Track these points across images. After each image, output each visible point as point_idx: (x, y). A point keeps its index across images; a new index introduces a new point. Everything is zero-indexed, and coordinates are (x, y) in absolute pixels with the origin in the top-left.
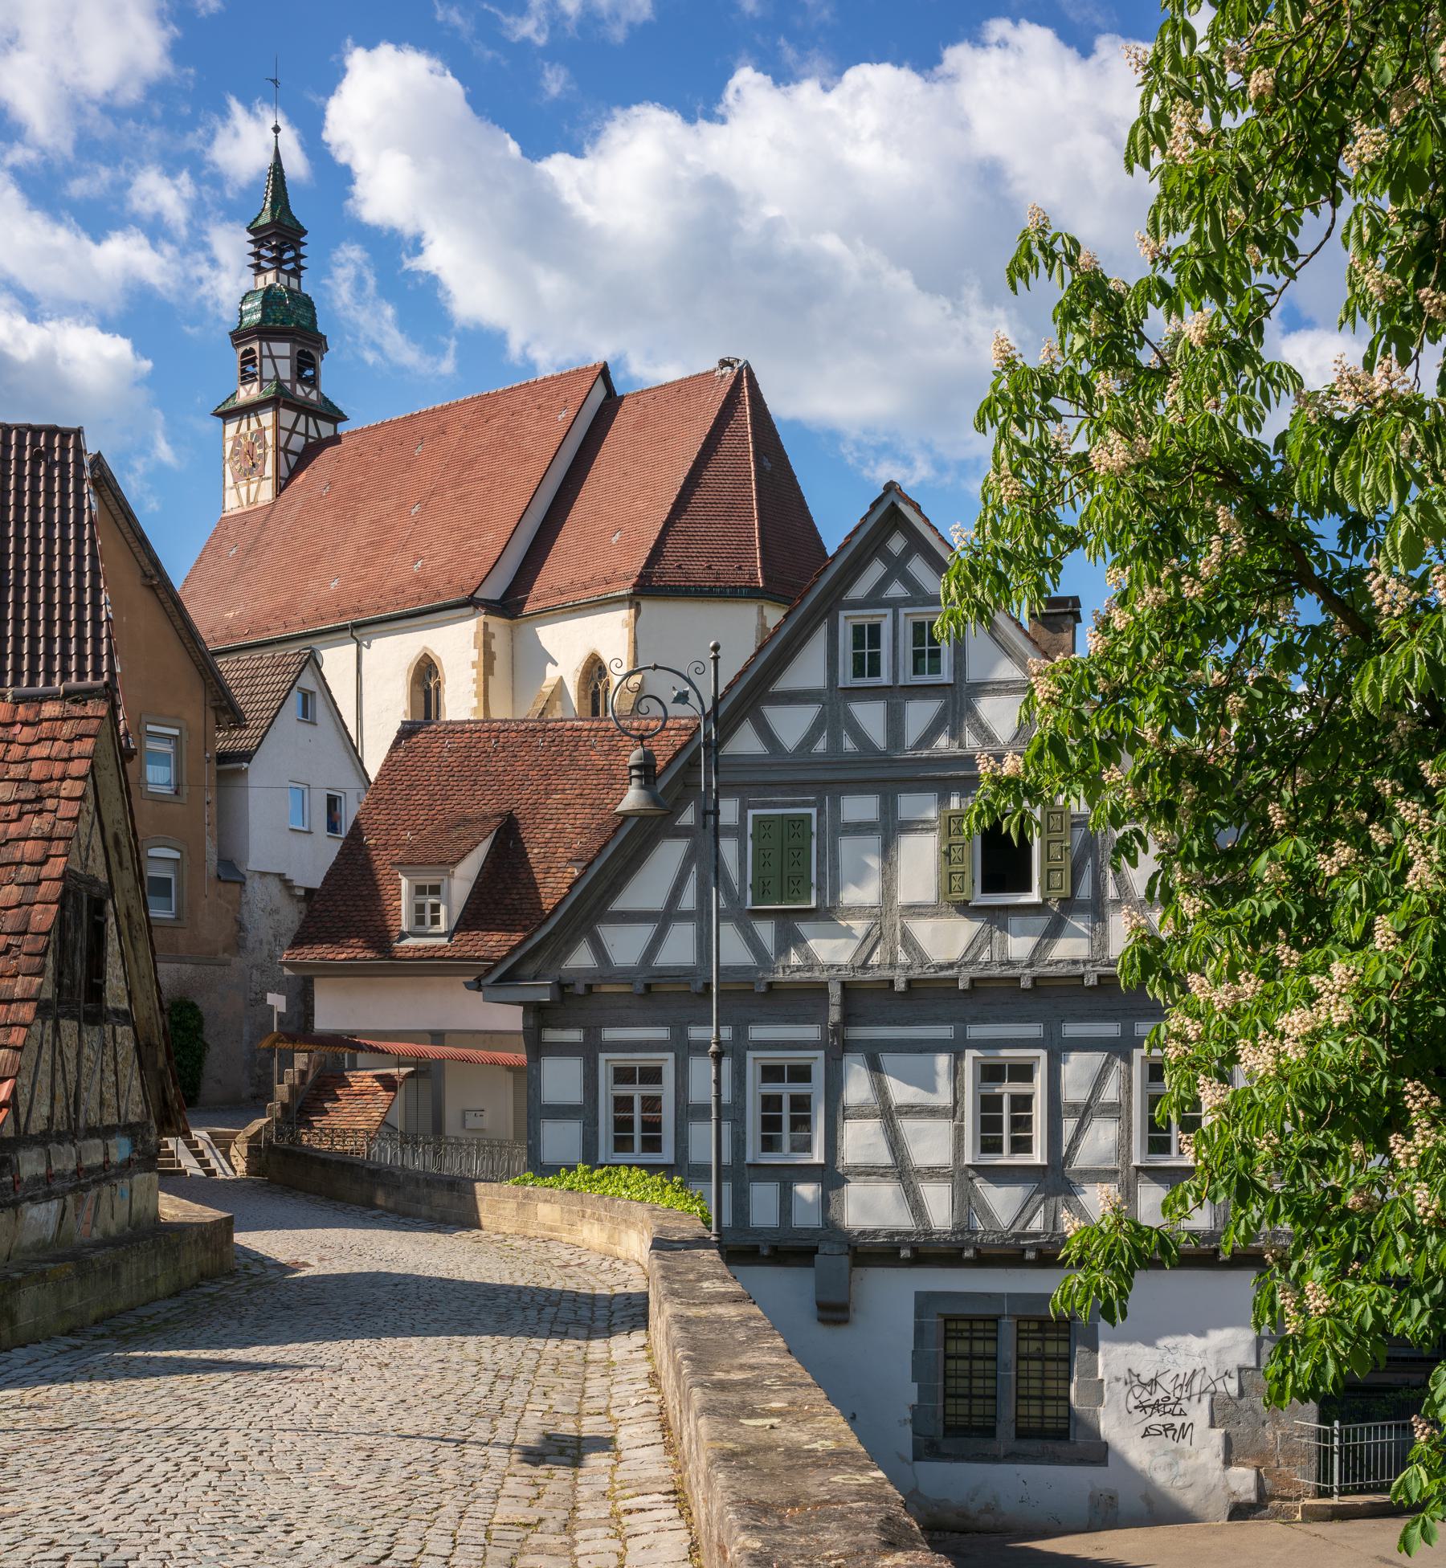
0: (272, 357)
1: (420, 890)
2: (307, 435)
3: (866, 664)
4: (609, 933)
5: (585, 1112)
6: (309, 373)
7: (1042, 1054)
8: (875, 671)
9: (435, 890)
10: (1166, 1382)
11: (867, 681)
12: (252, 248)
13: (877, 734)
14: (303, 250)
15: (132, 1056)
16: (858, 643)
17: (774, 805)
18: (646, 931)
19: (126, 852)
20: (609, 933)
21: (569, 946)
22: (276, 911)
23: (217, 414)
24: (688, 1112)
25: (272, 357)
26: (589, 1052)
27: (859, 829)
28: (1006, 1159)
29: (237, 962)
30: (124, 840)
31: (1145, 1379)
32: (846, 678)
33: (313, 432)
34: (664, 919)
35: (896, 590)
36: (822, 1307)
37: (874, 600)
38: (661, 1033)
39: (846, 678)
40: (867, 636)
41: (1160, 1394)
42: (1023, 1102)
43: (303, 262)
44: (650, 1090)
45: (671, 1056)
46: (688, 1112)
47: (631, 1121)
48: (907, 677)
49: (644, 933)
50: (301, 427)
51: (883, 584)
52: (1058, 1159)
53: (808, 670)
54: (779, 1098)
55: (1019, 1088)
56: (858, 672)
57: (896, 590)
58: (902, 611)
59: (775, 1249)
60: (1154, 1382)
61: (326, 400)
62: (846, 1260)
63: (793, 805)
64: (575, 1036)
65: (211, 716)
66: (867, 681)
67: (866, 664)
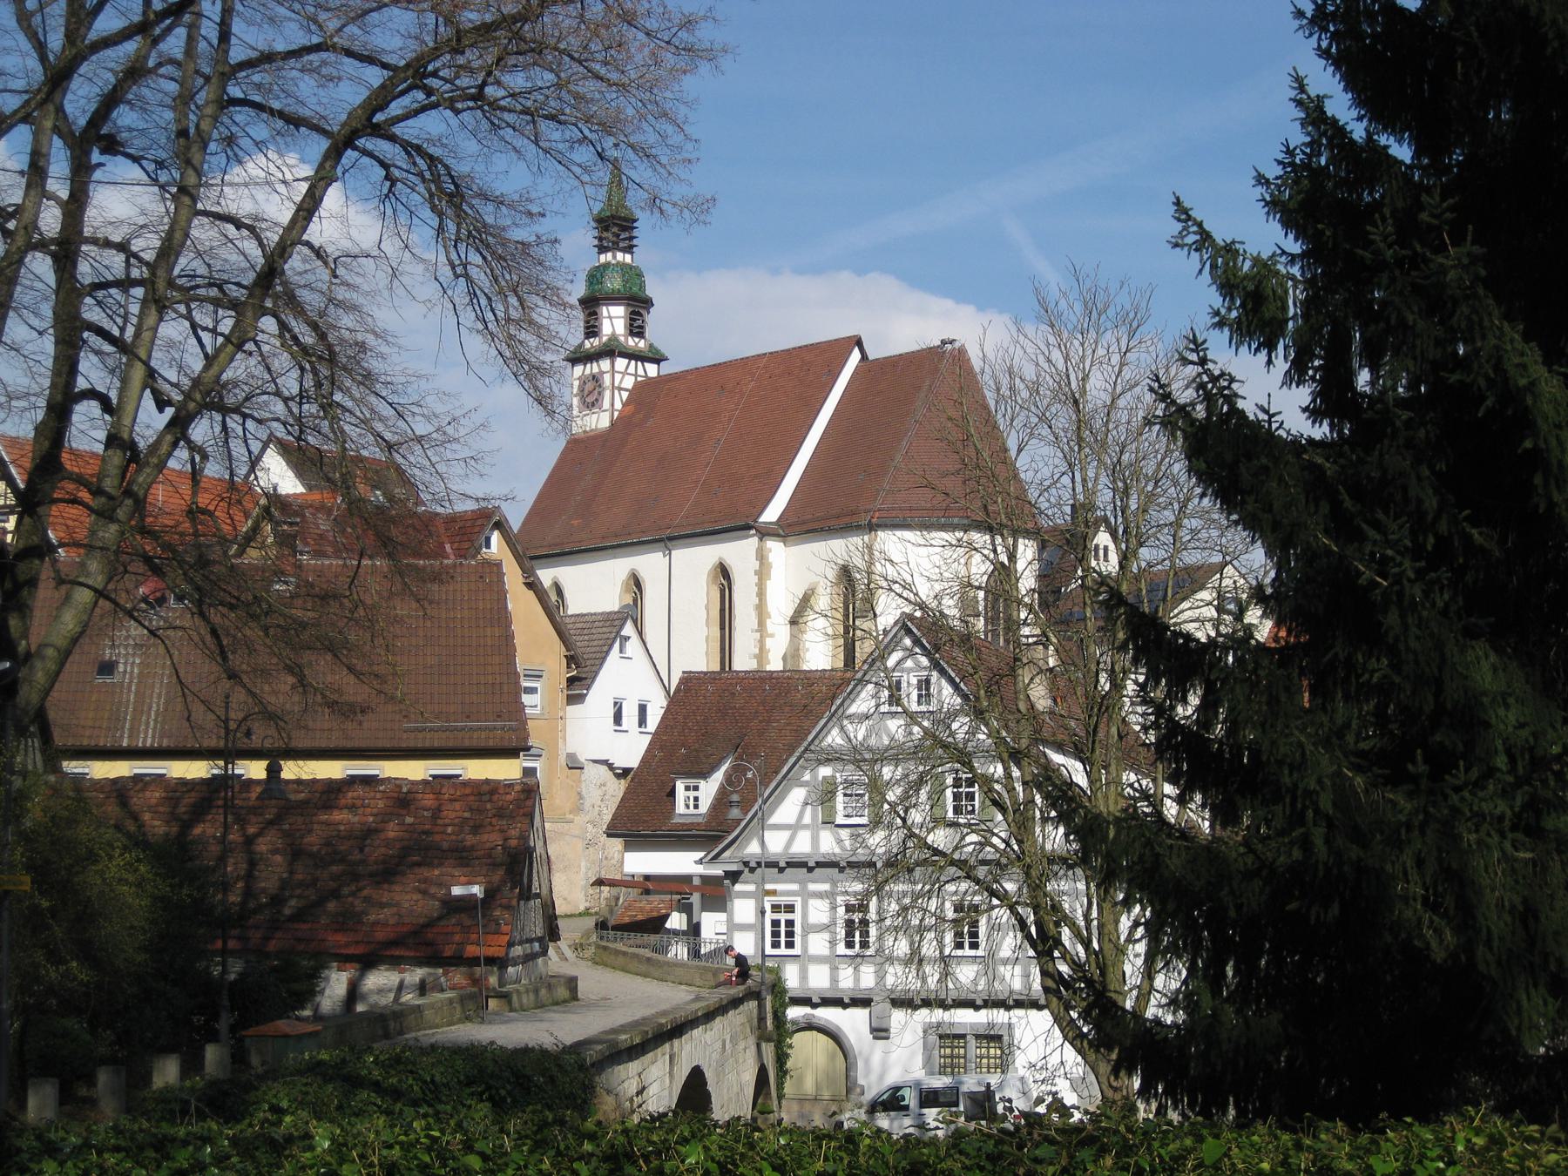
0: (610, 318)
1: (687, 788)
2: (636, 375)
9: (696, 788)
15: (991, 1025)
18: (786, 834)
21: (748, 841)
25: (610, 318)
29: (577, 819)
33: (641, 372)
34: (795, 828)
36: (874, 1030)
38: (795, 887)
42: (790, 923)
43: (635, 242)
44: (790, 916)
46: (808, 929)
49: (784, 835)
50: (631, 370)
52: (992, 954)
55: (790, 916)
61: (651, 346)
64: (751, 888)
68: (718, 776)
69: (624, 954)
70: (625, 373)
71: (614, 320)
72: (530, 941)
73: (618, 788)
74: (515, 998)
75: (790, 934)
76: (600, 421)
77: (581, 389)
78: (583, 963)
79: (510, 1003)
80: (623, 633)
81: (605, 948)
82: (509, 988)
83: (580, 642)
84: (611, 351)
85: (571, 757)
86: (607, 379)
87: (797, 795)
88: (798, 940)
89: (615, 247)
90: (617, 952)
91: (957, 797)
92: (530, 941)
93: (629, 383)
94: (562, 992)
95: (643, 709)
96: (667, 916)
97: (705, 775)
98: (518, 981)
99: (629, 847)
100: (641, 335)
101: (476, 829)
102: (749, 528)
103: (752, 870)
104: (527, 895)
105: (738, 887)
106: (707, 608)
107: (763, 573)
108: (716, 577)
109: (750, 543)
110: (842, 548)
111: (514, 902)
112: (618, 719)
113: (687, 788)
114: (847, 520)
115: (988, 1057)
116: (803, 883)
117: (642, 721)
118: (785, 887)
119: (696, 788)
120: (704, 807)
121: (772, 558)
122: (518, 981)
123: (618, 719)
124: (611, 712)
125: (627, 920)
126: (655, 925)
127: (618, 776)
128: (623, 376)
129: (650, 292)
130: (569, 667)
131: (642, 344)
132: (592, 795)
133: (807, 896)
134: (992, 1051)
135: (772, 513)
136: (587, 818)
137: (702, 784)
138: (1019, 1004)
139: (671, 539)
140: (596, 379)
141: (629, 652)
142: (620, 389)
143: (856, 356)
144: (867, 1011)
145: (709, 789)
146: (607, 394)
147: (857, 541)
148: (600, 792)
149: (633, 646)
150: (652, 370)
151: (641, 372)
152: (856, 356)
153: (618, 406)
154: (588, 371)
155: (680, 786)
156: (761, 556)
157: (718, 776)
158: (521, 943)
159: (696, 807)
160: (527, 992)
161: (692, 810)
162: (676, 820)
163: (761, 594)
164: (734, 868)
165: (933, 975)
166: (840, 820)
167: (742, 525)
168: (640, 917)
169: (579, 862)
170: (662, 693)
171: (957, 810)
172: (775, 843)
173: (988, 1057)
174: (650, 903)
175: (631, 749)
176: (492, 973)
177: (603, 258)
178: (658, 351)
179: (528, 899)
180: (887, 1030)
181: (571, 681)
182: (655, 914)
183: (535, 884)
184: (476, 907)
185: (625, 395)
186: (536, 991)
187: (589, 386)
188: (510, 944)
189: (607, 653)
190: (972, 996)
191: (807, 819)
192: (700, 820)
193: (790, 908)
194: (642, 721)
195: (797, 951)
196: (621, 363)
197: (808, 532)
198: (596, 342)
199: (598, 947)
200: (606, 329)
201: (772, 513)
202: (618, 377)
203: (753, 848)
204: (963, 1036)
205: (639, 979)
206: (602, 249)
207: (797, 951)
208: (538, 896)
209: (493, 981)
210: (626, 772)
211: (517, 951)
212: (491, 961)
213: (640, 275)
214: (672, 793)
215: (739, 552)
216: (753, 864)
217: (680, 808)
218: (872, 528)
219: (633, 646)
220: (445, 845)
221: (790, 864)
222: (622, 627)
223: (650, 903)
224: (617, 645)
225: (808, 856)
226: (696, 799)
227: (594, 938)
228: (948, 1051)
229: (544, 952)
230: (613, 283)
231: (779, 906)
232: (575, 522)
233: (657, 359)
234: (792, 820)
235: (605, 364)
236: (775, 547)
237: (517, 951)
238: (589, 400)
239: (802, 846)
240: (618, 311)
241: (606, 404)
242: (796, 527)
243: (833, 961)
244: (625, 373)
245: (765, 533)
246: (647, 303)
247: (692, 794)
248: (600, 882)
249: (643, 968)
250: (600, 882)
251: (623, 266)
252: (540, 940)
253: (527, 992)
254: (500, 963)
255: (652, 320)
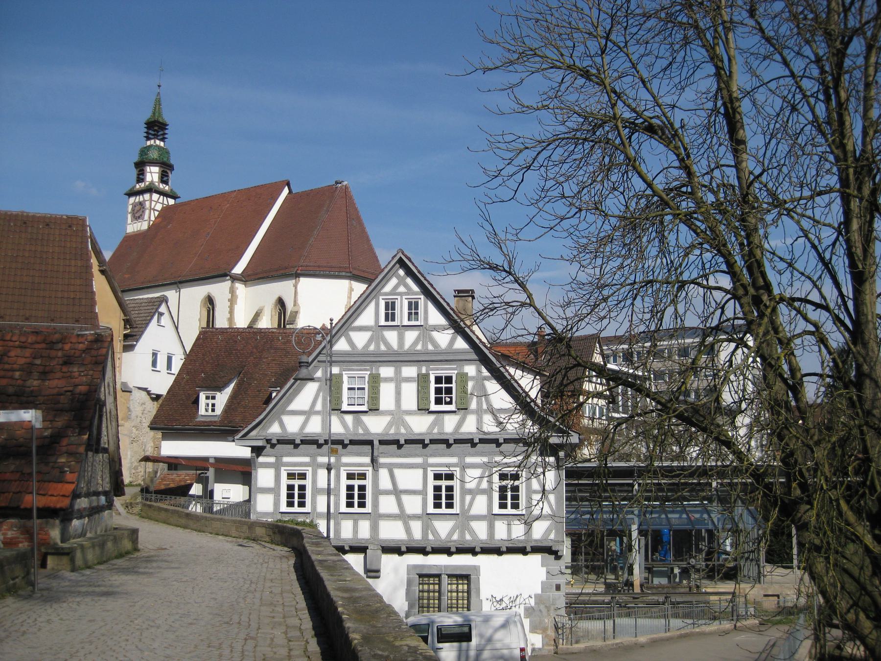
0: (151, 172)
1: (207, 398)
2: (163, 204)
3: (390, 316)
4: (286, 419)
5: (275, 491)
6: (165, 179)
7: (310, 469)
8: (393, 320)
9: (214, 398)
10: (506, 600)
11: (390, 323)
12: (146, 130)
13: (395, 345)
14: (166, 131)
16: (387, 308)
17: (353, 370)
19: (112, 390)
20: (286, 419)
21: (271, 424)
22: (144, 404)
23: (126, 194)
24: (316, 491)
25: (151, 172)
26: (277, 466)
27: (387, 380)
28: (444, 510)
30: (111, 385)
31: (498, 599)
32: (382, 322)
33: (165, 202)
34: (308, 414)
35: (402, 289)
37: (393, 292)
38: (307, 459)
39: (382, 322)
40: (390, 306)
41: (504, 605)
44: (302, 482)
45: (310, 469)
46: (316, 491)
47: (293, 494)
48: (406, 322)
49: (301, 419)
50: (161, 200)
51: (396, 287)
53: (367, 318)
54: (446, 507)
55: (302, 482)
56: (387, 319)
57: (402, 289)
58: (404, 297)
59: (350, 547)
60: (501, 600)
62: (380, 552)
63: (361, 370)
64: (272, 460)
65: (123, 323)
66: (390, 323)
67: (390, 316)
68: (229, 390)
69: (166, 510)
70: (157, 202)
71: (153, 174)
72: (97, 494)
73: (152, 408)
74: (79, 555)
75: (302, 496)
76: (144, 226)
77: (133, 210)
78: (133, 517)
79: (72, 560)
80: (160, 310)
81: (150, 506)
82: (73, 542)
83: (134, 315)
84: (150, 190)
85: (124, 384)
86: (147, 203)
87: (311, 389)
88: (369, 500)
89: (156, 137)
90: (160, 509)
91: (438, 391)
92: (97, 494)
93: (159, 207)
94: (127, 545)
95: (169, 359)
96: (190, 486)
97: (220, 388)
98: (83, 534)
99: (165, 437)
100: (166, 183)
101: (45, 374)
102: (226, 275)
103: (273, 446)
104: (95, 446)
105: (261, 459)
106: (200, 320)
107: (233, 301)
108: (205, 303)
109: (226, 284)
110: (282, 288)
111: (82, 449)
112: (154, 364)
113: (207, 398)
114: (282, 272)
115: (457, 592)
116: (313, 457)
117: (169, 366)
118: (296, 460)
119: (214, 398)
120: (219, 410)
121: (238, 292)
122: (83, 534)
123: (154, 364)
124: (150, 359)
125: (163, 487)
126: (183, 491)
127: (153, 399)
128: (156, 204)
129: (172, 162)
130: (125, 328)
131: (167, 188)
132: (136, 410)
133: (316, 466)
134: (460, 587)
135: (239, 269)
136: (133, 424)
137: (218, 395)
138: (486, 551)
139: (181, 282)
140: (141, 204)
141: (163, 323)
142: (154, 210)
143: (286, 191)
144: (362, 556)
145: (222, 398)
146: (147, 212)
147: (288, 284)
148: (141, 408)
149: (166, 320)
150: (171, 202)
151: (165, 202)
152: (286, 191)
153: (153, 218)
154: (137, 200)
155: (202, 396)
156: (232, 291)
157: (229, 390)
158: (88, 495)
159: (213, 410)
160: (93, 546)
161: (210, 413)
162: (199, 419)
163: (231, 312)
164: (260, 443)
165: (417, 528)
166: (345, 407)
167: (222, 274)
168: (172, 485)
169: (135, 440)
170: (182, 351)
171: (438, 401)
172: (292, 425)
173: (457, 592)
174: (179, 476)
175: (162, 384)
176: (53, 526)
177: (149, 143)
178: (175, 193)
179: (97, 451)
180: (378, 571)
181: (126, 337)
182: (183, 483)
183: (104, 439)
184: (27, 455)
185: (157, 213)
186: (102, 545)
187: (137, 208)
188: (76, 495)
189: (150, 320)
190: (448, 545)
191: (319, 407)
192: (216, 419)
193: (303, 476)
194: (169, 366)
195: (522, 510)
196: (155, 196)
197: (263, 278)
198: (142, 185)
199: (144, 505)
200: (148, 178)
201: (239, 269)
202: (153, 203)
203: (275, 429)
204: (439, 576)
205: (180, 530)
206: (148, 139)
207: (368, 509)
208: (105, 450)
209: (55, 534)
210: (158, 397)
211: (83, 503)
212: (48, 513)
213: (168, 153)
214: (196, 402)
215: (219, 290)
216: (274, 441)
217: (202, 411)
218: (297, 276)
219: (166, 320)
220: (11, 390)
221: (303, 442)
222: (160, 306)
223: (179, 476)
224: (156, 317)
225: (319, 435)
226: (213, 405)
227: (139, 499)
228: (426, 587)
229: (110, 506)
230: (154, 155)
231: (294, 474)
232: (127, 276)
233: (174, 197)
234: (306, 408)
235: (147, 196)
236: (240, 287)
237: (83, 503)
238: (137, 215)
239: (315, 427)
240: (156, 169)
241: (146, 217)
242: (251, 277)
243: (491, 518)
244: (157, 202)
245: (234, 279)
246: (171, 167)
247: (210, 402)
248: (146, 459)
249: (183, 521)
250: (146, 459)
251: (159, 147)
252: (106, 493)
253: (93, 546)
254: (64, 515)
255: (172, 176)
